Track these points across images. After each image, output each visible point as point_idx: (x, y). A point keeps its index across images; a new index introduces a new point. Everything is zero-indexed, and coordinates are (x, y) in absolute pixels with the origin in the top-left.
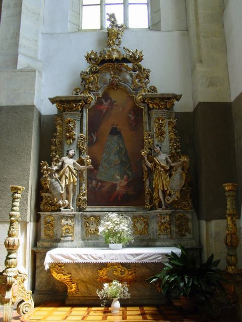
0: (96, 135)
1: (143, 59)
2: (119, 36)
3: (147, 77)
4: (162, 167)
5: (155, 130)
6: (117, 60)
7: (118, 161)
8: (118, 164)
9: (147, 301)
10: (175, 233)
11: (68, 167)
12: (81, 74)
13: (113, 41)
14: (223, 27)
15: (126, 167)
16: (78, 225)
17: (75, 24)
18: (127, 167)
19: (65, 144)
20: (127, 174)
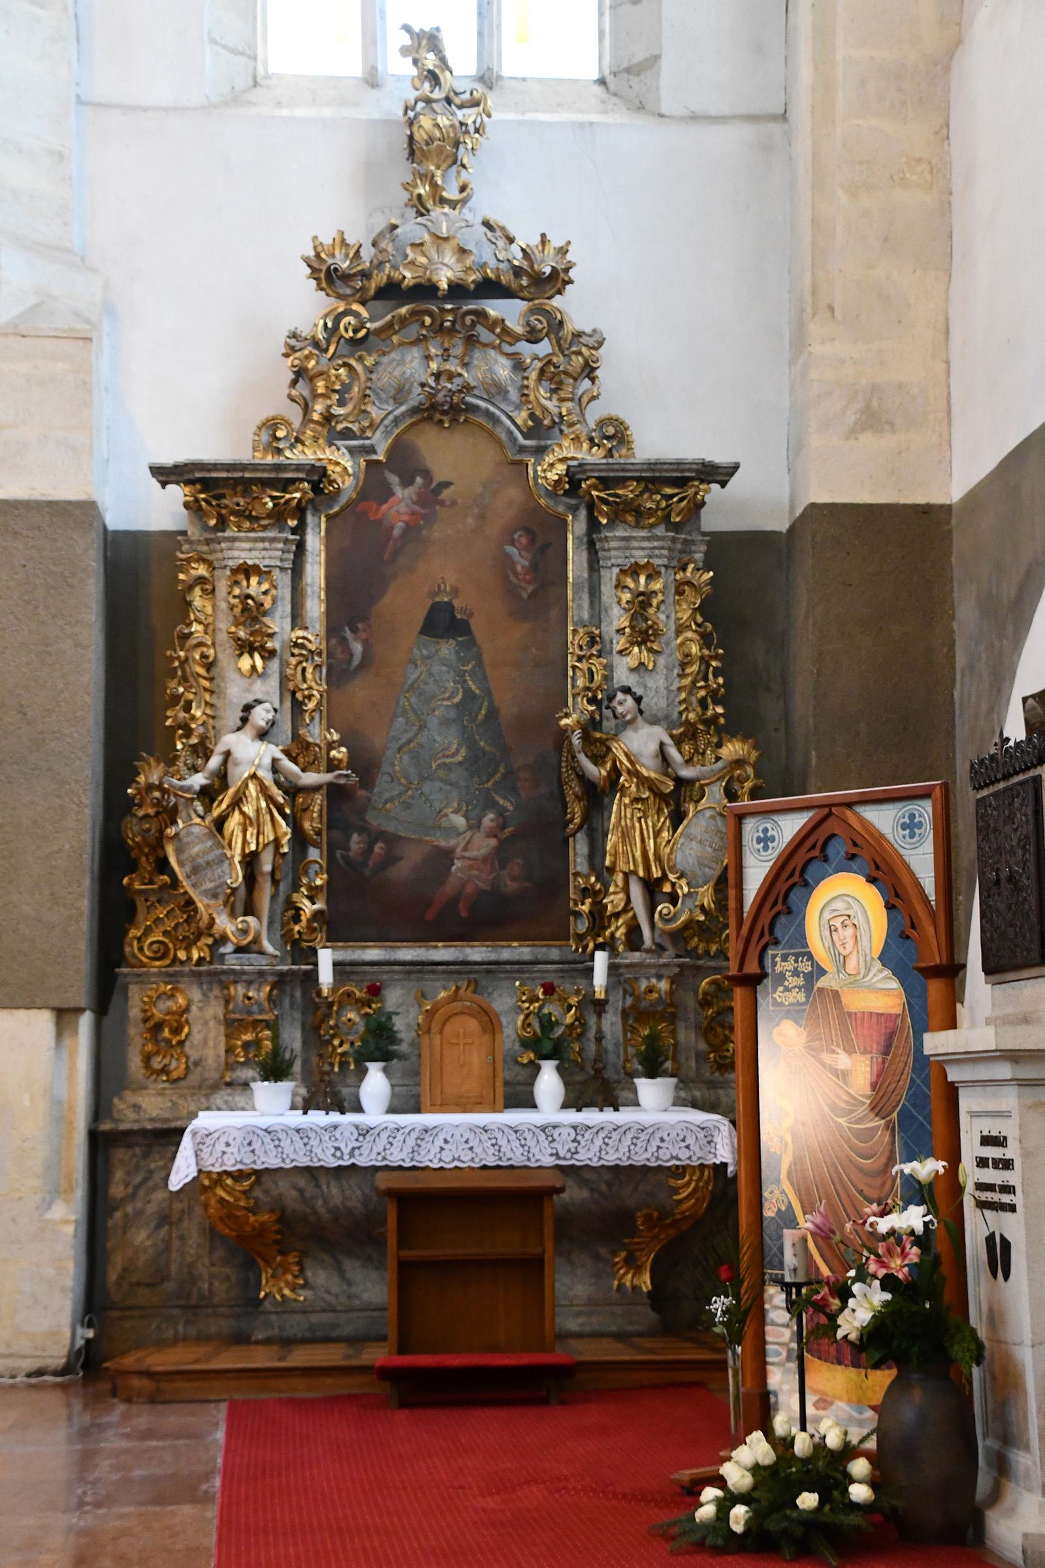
0: (364, 635)
1: (571, 282)
2: (464, 156)
3: (589, 370)
4: (643, 781)
5: (617, 618)
6: (457, 290)
7: (457, 751)
8: (460, 763)
9: (581, 1320)
10: (692, 1054)
11: (254, 776)
12: (291, 351)
13: (434, 185)
14: (943, 133)
15: (491, 776)
16: (292, 1023)
17: (234, 51)
18: (498, 777)
19: (232, 675)
20: (494, 805)
